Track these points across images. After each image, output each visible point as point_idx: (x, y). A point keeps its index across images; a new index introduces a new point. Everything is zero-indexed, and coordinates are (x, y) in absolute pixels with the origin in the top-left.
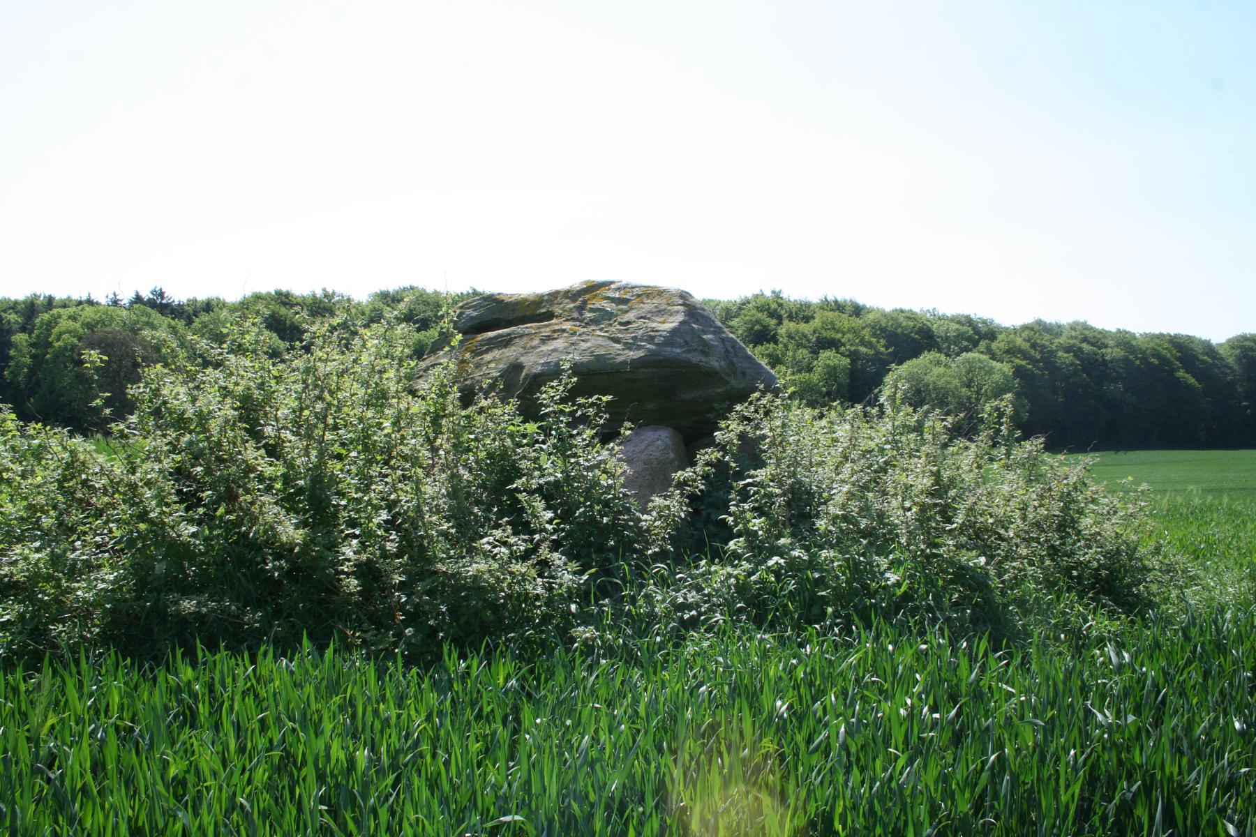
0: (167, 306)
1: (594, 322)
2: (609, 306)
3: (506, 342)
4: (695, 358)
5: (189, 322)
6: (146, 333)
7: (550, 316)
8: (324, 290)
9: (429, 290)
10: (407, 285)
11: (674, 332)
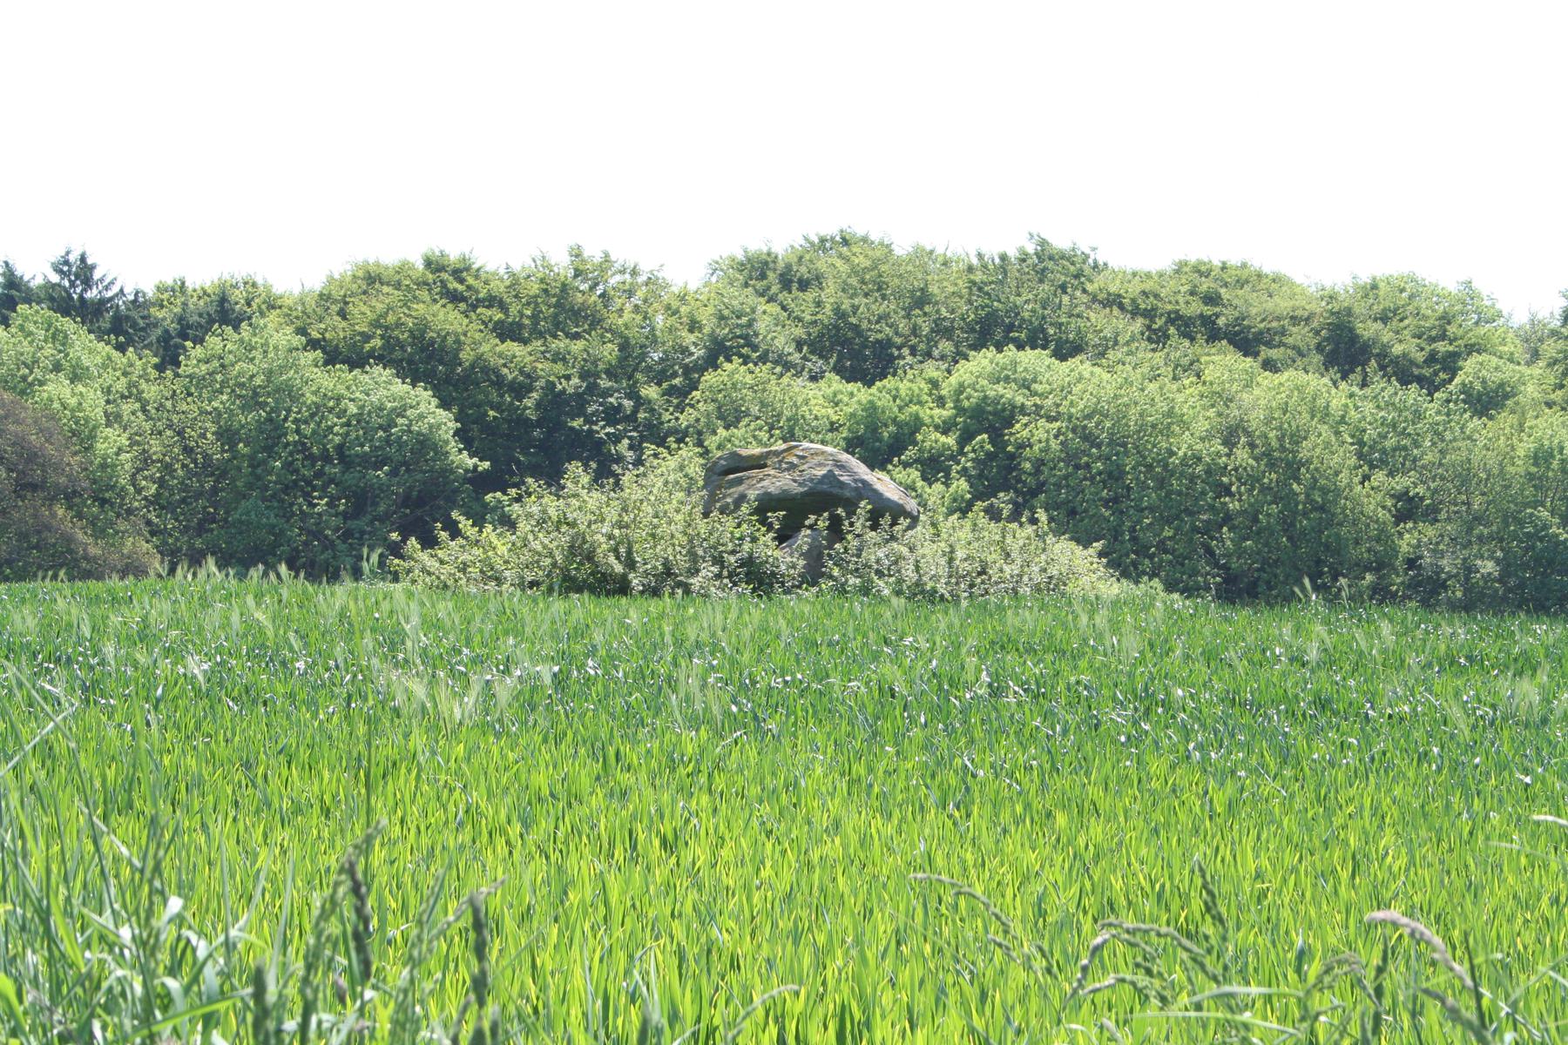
0: (100, 306)
1: (788, 470)
2: (795, 460)
3: (740, 481)
4: (836, 491)
5: (170, 358)
6: (58, 389)
7: (765, 466)
8: (577, 254)
9: (902, 248)
10: (831, 230)
11: (824, 476)
